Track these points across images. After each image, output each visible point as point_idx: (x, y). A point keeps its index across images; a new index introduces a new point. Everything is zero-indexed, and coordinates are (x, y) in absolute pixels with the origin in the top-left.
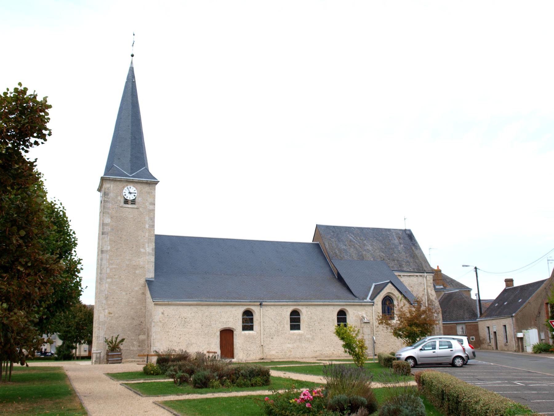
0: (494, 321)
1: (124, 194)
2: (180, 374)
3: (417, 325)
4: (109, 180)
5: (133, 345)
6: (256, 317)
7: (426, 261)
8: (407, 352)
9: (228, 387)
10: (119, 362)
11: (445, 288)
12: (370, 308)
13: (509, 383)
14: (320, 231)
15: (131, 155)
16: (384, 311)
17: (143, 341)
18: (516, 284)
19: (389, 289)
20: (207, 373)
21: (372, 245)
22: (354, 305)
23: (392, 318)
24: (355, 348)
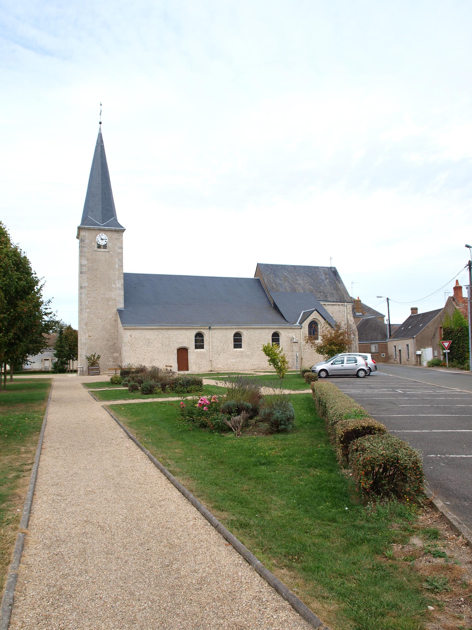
0: (399, 342)
1: (97, 240)
2: (132, 383)
3: (336, 345)
4: (85, 229)
5: (109, 361)
6: (206, 338)
7: (347, 293)
8: (322, 365)
9: (169, 393)
10: (98, 374)
11: (363, 314)
12: (299, 330)
13: (392, 391)
14: (261, 268)
15: (102, 208)
16: (310, 333)
17: (117, 358)
18: (419, 312)
19: (315, 315)
20: (152, 382)
21: (303, 280)
22: (285, 328)
23: (317, 338)
24: (278, 363)
